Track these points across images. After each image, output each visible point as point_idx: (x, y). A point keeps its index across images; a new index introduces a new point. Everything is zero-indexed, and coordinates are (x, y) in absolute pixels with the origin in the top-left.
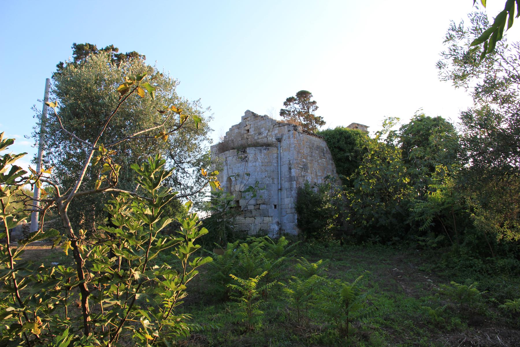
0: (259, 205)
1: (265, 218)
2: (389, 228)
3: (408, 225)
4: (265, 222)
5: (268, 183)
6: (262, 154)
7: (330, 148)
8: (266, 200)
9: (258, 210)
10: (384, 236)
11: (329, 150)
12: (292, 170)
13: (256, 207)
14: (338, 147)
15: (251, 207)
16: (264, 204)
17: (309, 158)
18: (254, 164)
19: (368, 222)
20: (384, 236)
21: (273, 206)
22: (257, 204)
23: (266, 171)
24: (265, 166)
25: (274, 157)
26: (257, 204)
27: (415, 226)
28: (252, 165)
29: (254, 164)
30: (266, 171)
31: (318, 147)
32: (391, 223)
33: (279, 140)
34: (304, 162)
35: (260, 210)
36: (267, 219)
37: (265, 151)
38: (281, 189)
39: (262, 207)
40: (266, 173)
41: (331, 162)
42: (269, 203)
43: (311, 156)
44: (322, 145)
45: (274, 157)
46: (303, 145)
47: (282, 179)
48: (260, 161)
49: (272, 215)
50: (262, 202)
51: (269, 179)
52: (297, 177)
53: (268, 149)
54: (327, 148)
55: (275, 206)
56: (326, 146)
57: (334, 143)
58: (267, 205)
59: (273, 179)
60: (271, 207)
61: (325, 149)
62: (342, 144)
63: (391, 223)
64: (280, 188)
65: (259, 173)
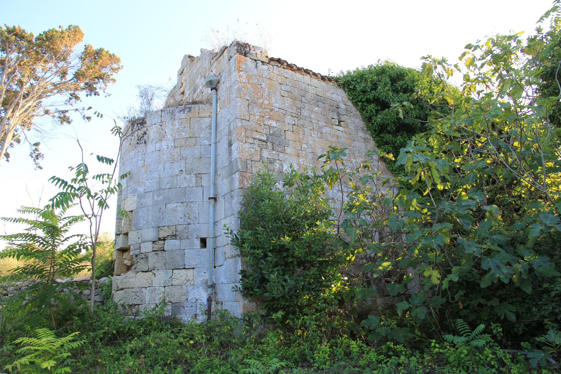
0: (164, 240)
1: (175, 271)
2: (529, 290)
3: (94, 312)
4: (175, 282)
5: (186, 185)
6: (176, 123)
7: (355, 104)
8: (179, 228)
9: (160, 253)
10: (512, 318)
11: (354, 109)
12: (234, 147)
13: (157, 247)
14: (374, 98)
15: (147, 247)
16: (174, 236)
17: (288, 119)
18: (158, 146)
19: (446, 272)
20: (512, 318)
21: (198, 243)
22: (160, 239)
23: (183, 158)
24: (181, 147)
25: (204, 126)
26: (160, 239)
27: (307, 272)
28: (153, 149)
29: (158, 146)
30: (183, 158)
31: (319, 100)
32: (531, 270)
33: (214, 86)
34: (270, 127)
35: (164, 253)
36: (181, 275)
37: (183, 115)
38: (215, 199)
39: (170, 244)
40: (183, 162)
41: (361, 134)
42: (185, 235)
43: (298, 116)
44: (334, 96)
45: (204, 126)
46: (270, 88)
47: (219, 172)
48: (169, 136)
49: (193, 264)
50: (170, 233)
51: (188, 177)
52: (246, 163)
53: (190, 108)
54: (350, 103)
55: (203, 242)
56: (346, 99)
57: (364, 92)
58: (181, 239)
59: (198, 175)
60: (192, 244)
61: (342, 106)
62: (384, 91)
63: (531, 270)
64: (212, 196)
65: (167, 165)
